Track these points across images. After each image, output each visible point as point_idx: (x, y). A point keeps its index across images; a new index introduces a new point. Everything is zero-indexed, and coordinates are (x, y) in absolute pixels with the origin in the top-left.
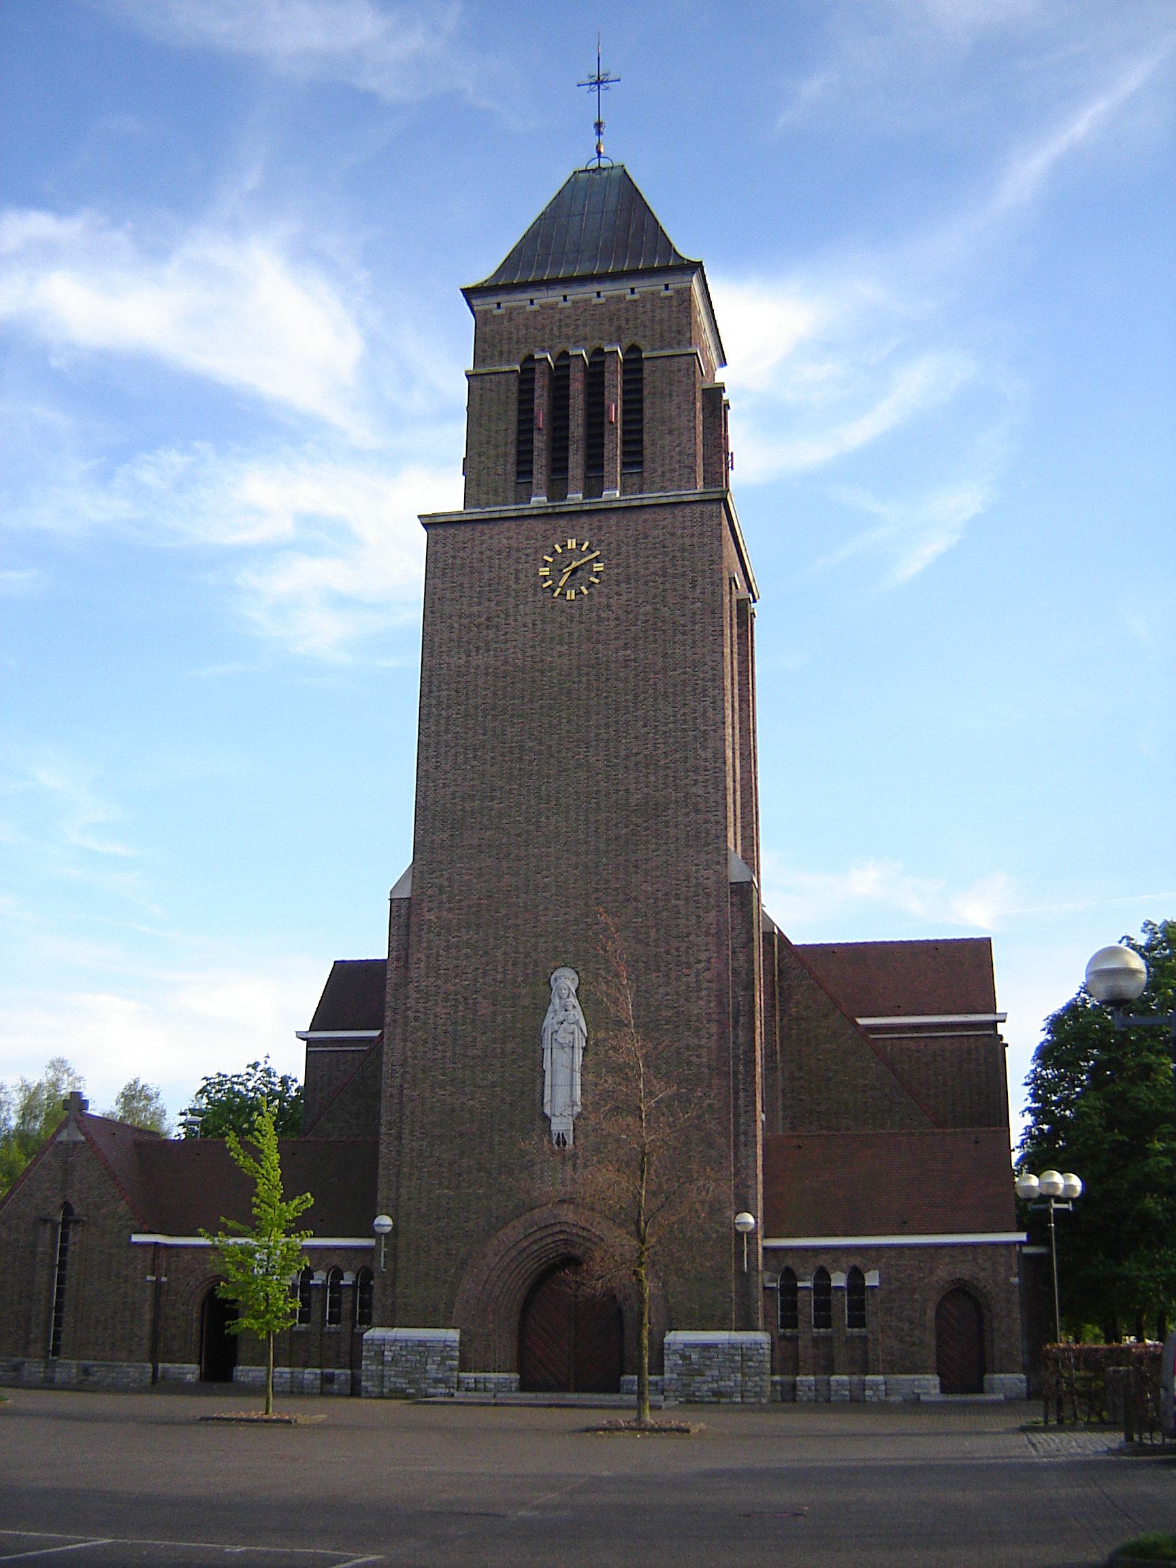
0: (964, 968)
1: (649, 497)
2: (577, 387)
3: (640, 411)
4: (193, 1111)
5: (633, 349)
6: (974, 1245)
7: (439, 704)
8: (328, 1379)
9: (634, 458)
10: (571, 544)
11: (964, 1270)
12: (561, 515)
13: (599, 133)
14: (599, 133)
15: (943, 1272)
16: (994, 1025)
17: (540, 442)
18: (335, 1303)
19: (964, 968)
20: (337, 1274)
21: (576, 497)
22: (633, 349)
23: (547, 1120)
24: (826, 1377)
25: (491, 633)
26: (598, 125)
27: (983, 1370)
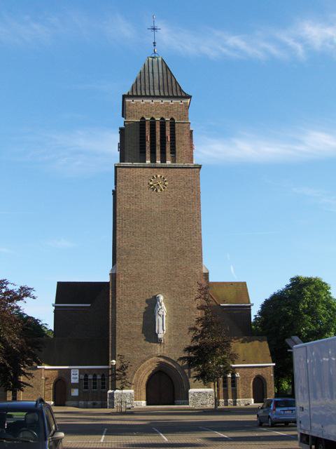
0: (241, 289)
1: (177, 164)
2: (158, 129)
3: (175, 138)
4: (189, 349)
5: (172, 119)
6: (248, 363)
7: (122, 219)
8: (94, 404)
9: (173, 151)
10: (159, 176)
11: (259, 372)
12: (156, 167)
13: (155, 45)
14: (155, 45)
15: (255, 373)
16: (250, 307)
17: (148, 144)
18: (95, 384)
19: (241, 289)
20: (95, 375)
21: (158, 162)
22: (172, 119)
23: (157, 335)
24: (252, 395)
25: (136, 200)
26: (154, 43)
27: (66, 400)
